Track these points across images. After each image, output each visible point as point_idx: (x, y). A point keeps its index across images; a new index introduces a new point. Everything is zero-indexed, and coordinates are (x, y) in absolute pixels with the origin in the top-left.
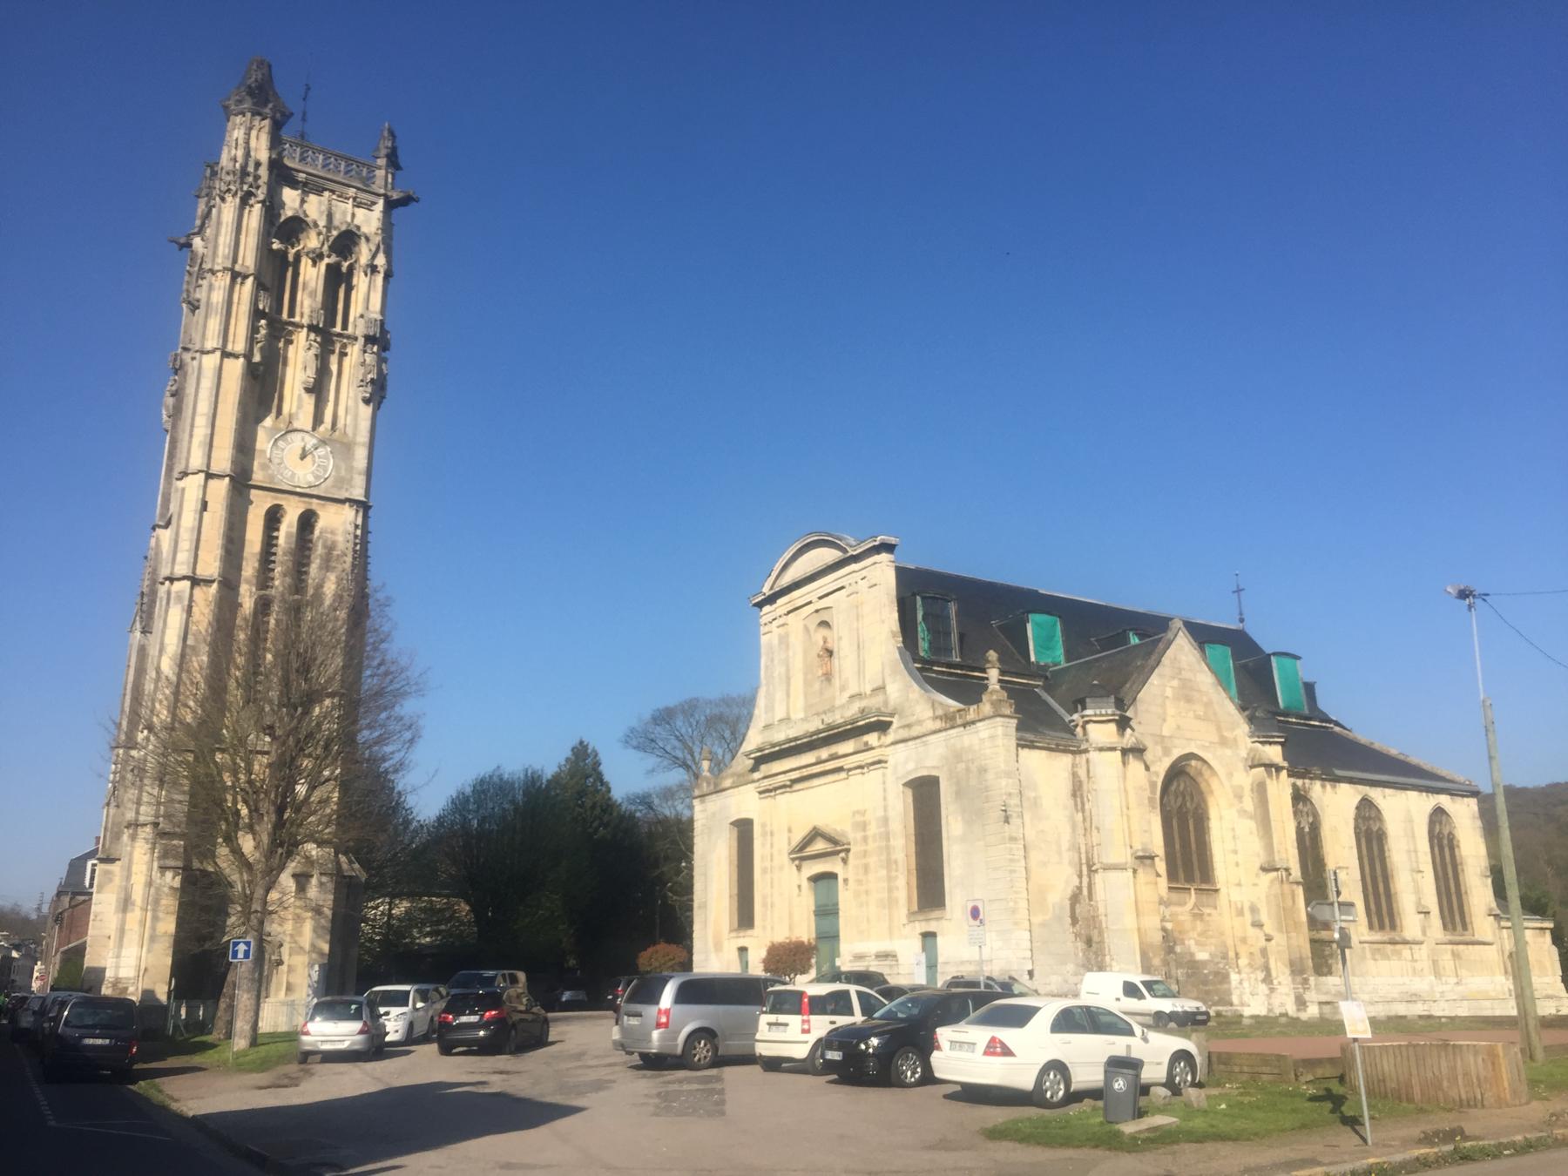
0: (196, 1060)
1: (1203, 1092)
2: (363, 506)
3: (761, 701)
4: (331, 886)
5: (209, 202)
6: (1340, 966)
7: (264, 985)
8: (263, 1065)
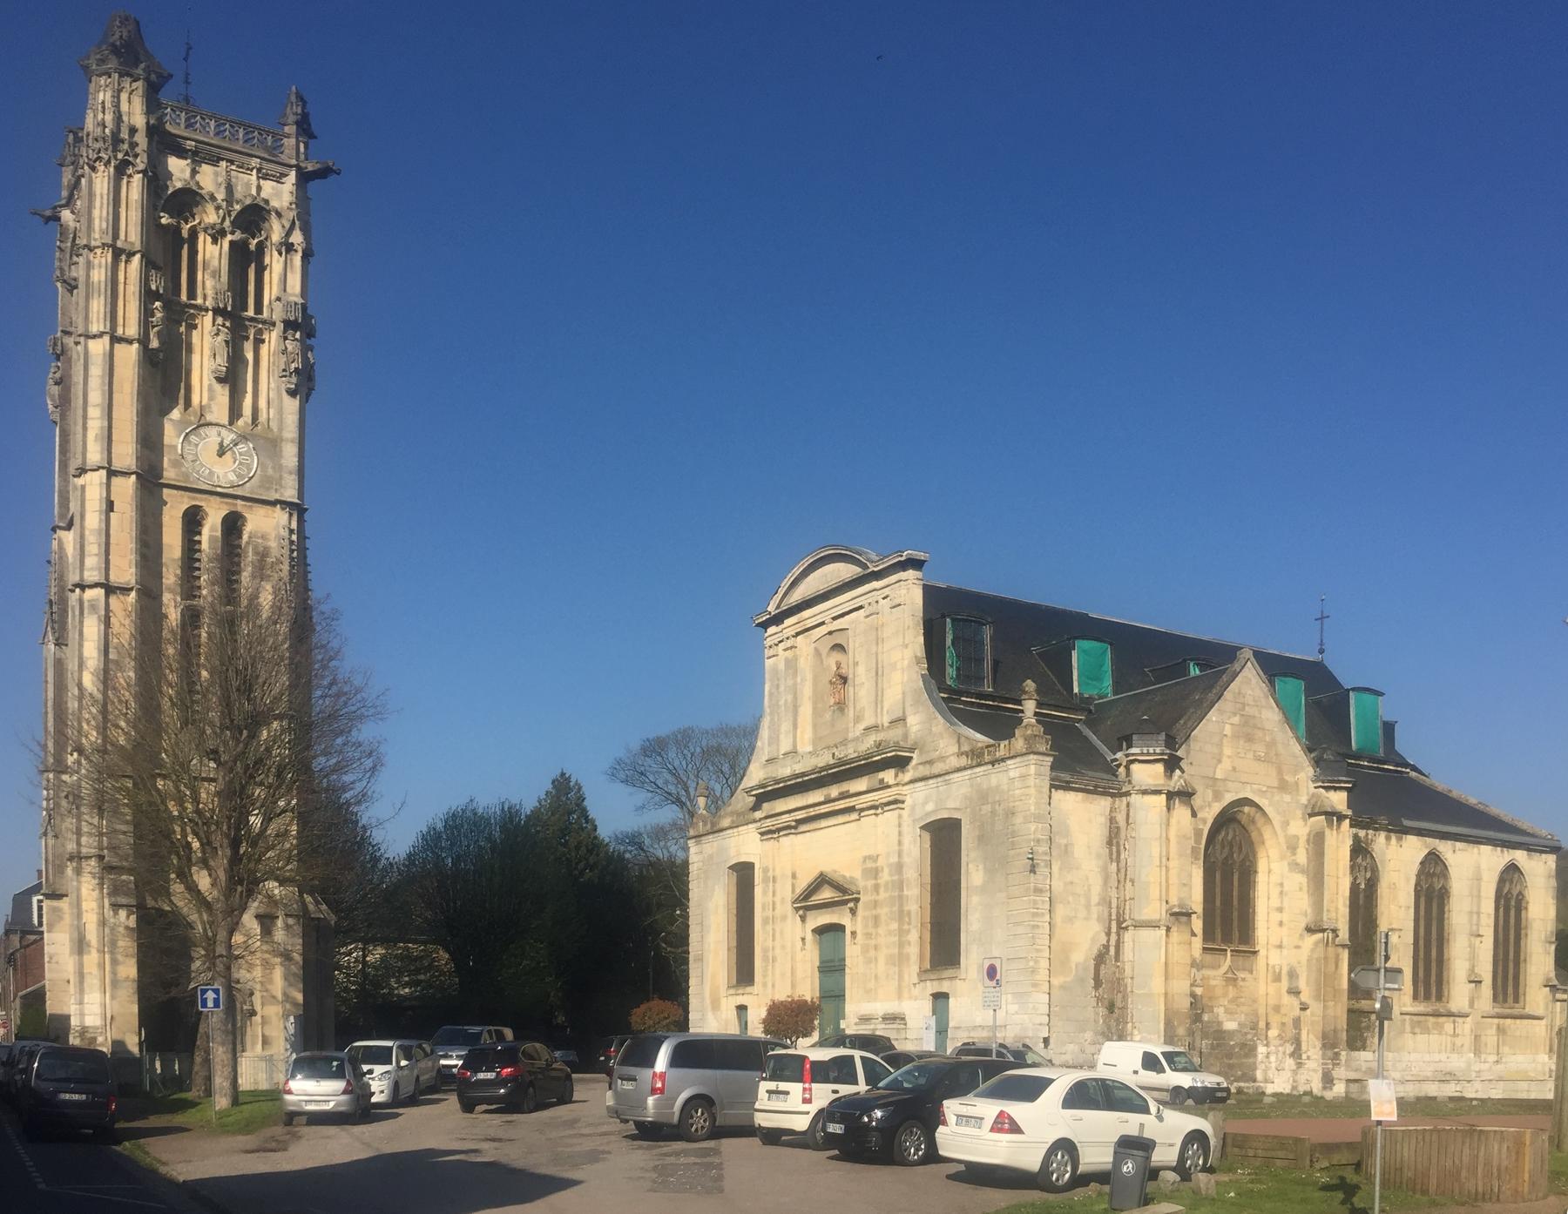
0: (179, 1119)
1: (1213, 1178)
2: (297, 509)
3: (764, 733)
4: (298, 929)
5: (76, 170)
6: (1376, 1040)
7: (239, 1038)
8: (247, 1127)
